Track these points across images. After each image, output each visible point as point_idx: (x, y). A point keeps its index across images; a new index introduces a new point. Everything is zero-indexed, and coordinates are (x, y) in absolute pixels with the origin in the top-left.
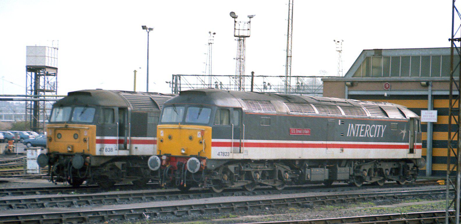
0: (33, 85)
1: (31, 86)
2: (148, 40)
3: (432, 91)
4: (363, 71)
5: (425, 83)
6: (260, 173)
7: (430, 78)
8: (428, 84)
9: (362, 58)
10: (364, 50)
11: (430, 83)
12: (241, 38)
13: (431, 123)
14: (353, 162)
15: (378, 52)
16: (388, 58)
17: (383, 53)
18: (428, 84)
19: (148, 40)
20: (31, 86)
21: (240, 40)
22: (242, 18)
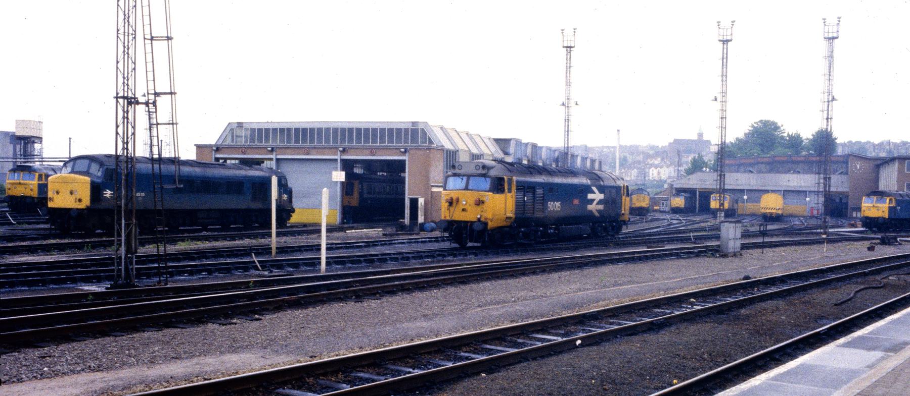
0: (22, 150)
1: (20, 151)
2: (70, 147)
3: (276, 155)
4: (229, 139)
5: (270, 149)
6: (631, 217)
7: (370, 144)
8: (405, 152)
9: (229, 129)
10: (230, 123)
11: (275, 149)
12: (725, 42)
13: (340, 182)
14: (325, 190)
15: (240, 125)
16: (247, 129)
17: (244, 125)
18: (405, 152)
19: (70, 147)
20: (20, 151)
21: (724, 44)
22: (569, 32)
